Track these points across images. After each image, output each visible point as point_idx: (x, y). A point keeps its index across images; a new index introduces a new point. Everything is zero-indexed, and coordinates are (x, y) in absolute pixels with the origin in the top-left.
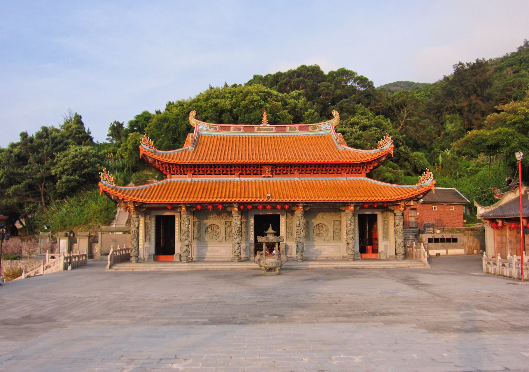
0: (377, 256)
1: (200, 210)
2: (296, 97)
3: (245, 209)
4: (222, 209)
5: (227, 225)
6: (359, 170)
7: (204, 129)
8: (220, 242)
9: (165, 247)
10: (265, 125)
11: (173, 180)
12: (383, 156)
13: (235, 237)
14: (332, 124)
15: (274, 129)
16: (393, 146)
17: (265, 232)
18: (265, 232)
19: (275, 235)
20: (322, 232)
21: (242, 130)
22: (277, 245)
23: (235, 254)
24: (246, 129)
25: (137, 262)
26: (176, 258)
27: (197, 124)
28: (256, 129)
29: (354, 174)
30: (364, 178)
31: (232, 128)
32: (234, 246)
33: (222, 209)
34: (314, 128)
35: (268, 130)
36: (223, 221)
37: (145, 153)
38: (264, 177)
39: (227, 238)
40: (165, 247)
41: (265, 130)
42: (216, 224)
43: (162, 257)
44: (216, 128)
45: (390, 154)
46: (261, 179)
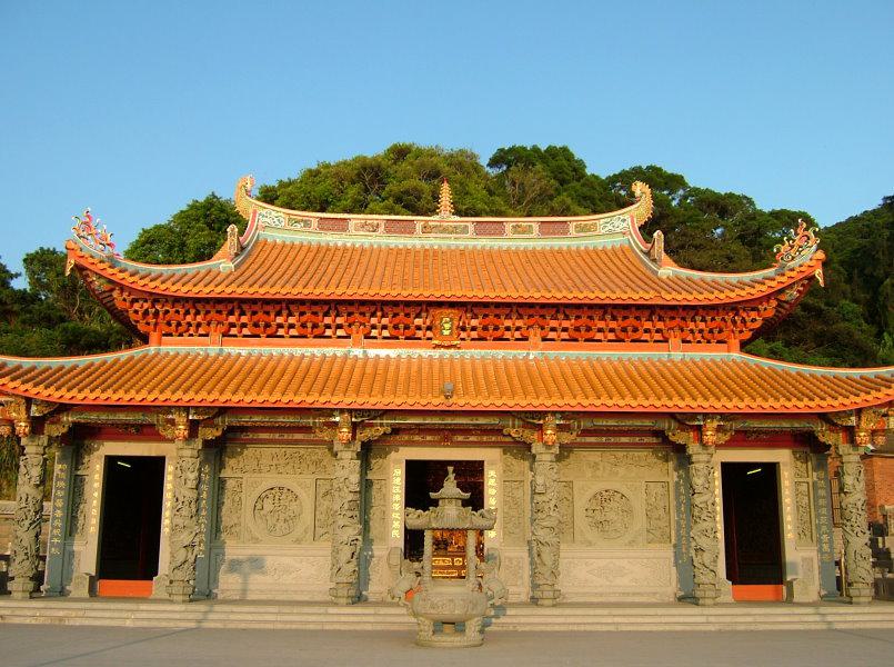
0: (779, 593)
1: (226, 434)
2: (537, 179)
3: (375, 431)
4: (295, 424)
5: (322, 491)
6: (721, 331)
7: (275, 226)
8: (298, 541)
9: (130, 549)
10: (445, 216)
11: (164, 349)
12: (790, 286)
13: (341, 523)
14: (632, 218)
15: (471, 227)
16: (821, 255)
17: (433, 495)
18: (433, 495)
19: (465, 503)
20: (611, 516)
21: (382, 229)
22: (472, 539)
23: (340, 579)
24: (391, 228)
25: (35, 593)
26: (158, 585)
27: (255, 213)
28: (419, 227)
29: (704, 344)
30: (737, 355)
31: (352, 224)
32: (336, 551)
33: (295, 424)
34: (581, 229)
35: (455, 230)
36: (309, 479)
37: (82, 262)
38: (437, 346)
39: (320, 531)
40: (130, 549)
41: (445, 230)
42: (287, 486)
43: (106, 585)
44: (307, 223)
45: (812, 278)
46: (425, 353)
